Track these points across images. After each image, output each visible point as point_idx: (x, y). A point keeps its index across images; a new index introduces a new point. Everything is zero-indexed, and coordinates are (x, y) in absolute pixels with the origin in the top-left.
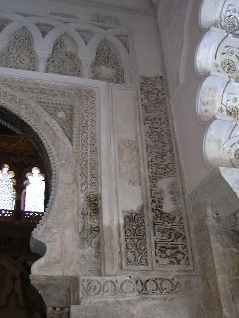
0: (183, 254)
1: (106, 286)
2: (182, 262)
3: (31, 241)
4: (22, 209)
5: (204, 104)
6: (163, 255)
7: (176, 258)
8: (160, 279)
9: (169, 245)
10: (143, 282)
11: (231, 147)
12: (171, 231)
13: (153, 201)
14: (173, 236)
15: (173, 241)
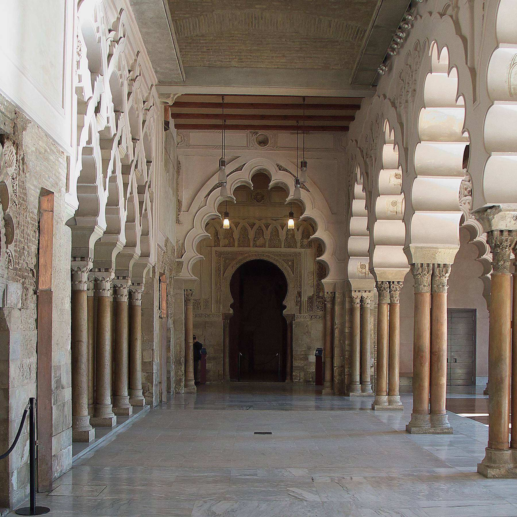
6: (318, 309)
13: (317, 293)
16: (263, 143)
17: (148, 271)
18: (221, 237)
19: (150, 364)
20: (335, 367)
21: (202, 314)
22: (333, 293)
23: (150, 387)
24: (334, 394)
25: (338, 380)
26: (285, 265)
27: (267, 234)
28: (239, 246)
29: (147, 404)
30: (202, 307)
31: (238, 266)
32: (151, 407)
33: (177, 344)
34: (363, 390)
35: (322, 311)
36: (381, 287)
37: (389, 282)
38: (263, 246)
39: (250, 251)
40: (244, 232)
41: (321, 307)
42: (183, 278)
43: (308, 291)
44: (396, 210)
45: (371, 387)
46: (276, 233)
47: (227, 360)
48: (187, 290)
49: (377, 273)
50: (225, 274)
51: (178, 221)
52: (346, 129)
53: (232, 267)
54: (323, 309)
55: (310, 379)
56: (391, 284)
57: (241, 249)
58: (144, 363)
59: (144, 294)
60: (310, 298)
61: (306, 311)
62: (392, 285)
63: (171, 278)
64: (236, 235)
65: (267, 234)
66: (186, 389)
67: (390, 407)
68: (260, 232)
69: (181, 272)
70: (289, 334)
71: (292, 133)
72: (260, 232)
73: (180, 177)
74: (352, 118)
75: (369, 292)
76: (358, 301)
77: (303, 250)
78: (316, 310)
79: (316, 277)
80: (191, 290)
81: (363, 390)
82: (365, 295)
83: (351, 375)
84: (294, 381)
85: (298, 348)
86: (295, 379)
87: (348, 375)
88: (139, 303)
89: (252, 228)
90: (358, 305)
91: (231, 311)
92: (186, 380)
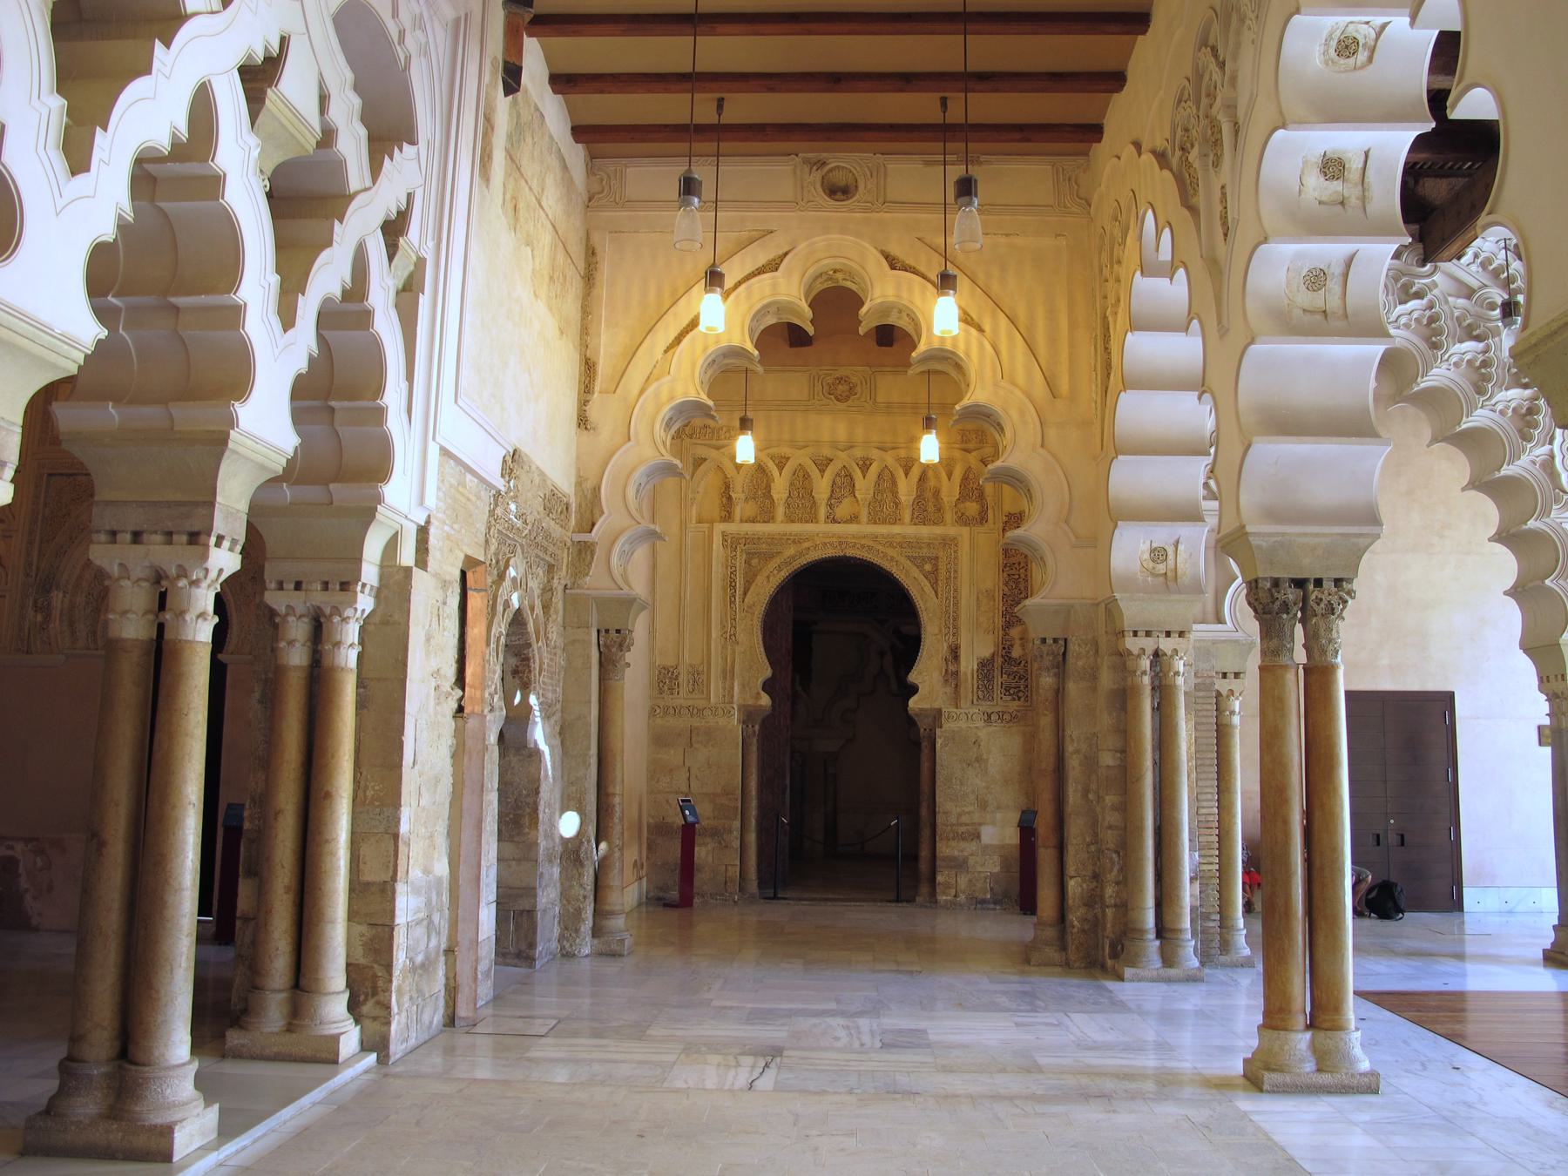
2: (1022, 699)
6: (1007, 693)
9: (1013, 685)
13: (1004, 648)
16: (839, 191)
17: (392, 546)
18: (737, 494)
19: (383, 891)
20: (1071, 877)
21: (681, 707)
22: (1062, 642)
23: (380, 983)
24: (1067, 966)
25: (1083, 920)
26: (915, 572)
27: (864, 486)
28: (790, 519)
29: (365, 1047)
30: (684, 690)
31: (784, 574)
32: (383, 1059)
33: (569, 800)
34: (1168, 959)
35: (1019, 700)
36: (1273, 603)
37: (1300, 583)
38: (854, 519)
39: (818, 535)
40: (802, 485)
41: (1015, 688)
42: (593, 593)
43: (977, 648)
44: (1322, 304)
45: (1192, 950)
46: (886, 482)
47: (752, 837)
48: (607, 631)
49: (1260, 547)
50: (748, 596)
51: (583, 422)
52: (1092, 132)
53: (768, 577)
54: (1021, 694)
55: (985, 893)
56: (1311, 587)
57: (796, 528)
58: (357, 887)
59: (375, 624)
60: (985, 666)
61: (975, 700)
62: (1316, 593)
63: (549, 590)
64: (780, 486)
65: (864, 486)
66: (596, 941)
67: (1326, 1078)
68: (844, 485)
69: (587, 575)
70: (925, 765)
71: (927, 163)
72: (844, 485)
73: (595, 292)
74: (1115, 80)
75: (1181, 634)
76: (1145, 663)
77: (965, 531)
78: (1001, 698)
79: (1001, 605)
80: (618, 631)
81: (1168, 959)
82: (1166, 645)
83: (1126, 907)
84: (939, 898)
85: (954, 804)
86: (944, 893)
87: (1116, 906)
88: (349, 657)
89: (822, 471)
90: (1146, 680)
91: (765, 700)
92: (598, 913)
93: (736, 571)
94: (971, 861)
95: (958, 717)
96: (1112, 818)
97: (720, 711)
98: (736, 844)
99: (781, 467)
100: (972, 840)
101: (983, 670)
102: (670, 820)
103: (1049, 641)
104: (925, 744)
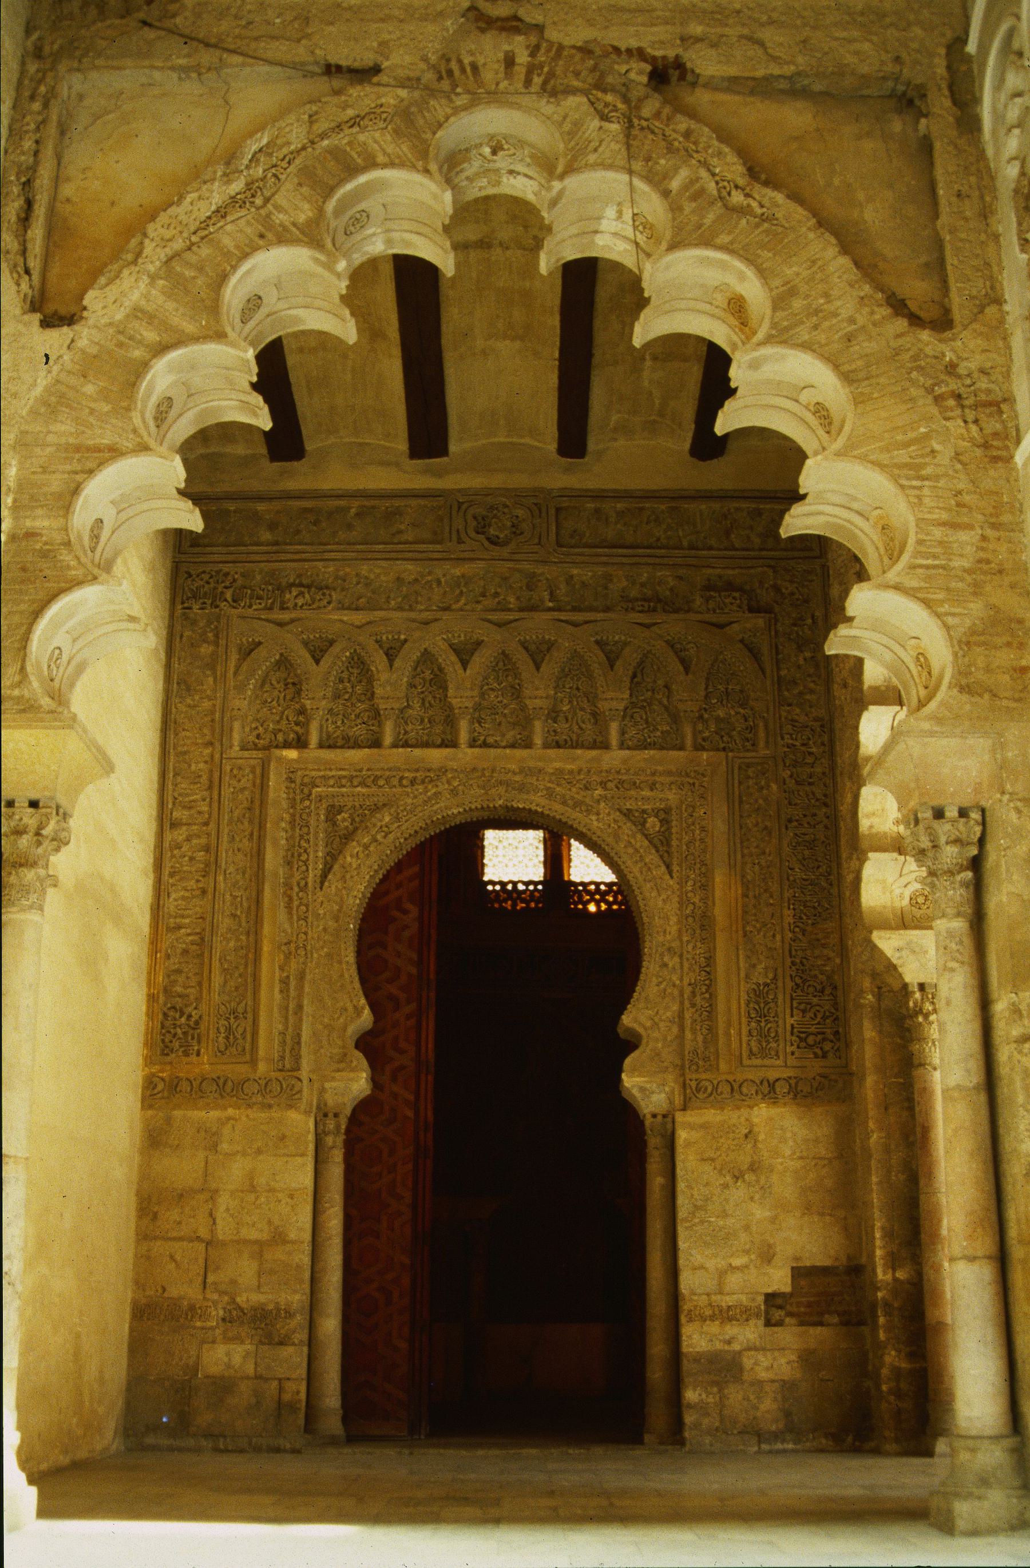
0: (832, 1041)
1: (720, 1086)
2: (831, 1055)
3: (619, 1026)
4: (566, 878)
5: (868, 816)
6: (803, 1044)
7: (821, 1049)
8: (795, 1078)
9: (813, 1029)
10: (771, 1082)
11: (905, 886)
12: (818, 1008)
13: (793, 963)
14: (819, 1016)
15: (818, 1023)
22: (975, 815)
54: (827, 1046)
70: (656, 1182)
80: (34, 804)
93: (308, 834)
94: (747, 1362)
95: (715, 1088)
96: (892, 1358)
97: (275, 1087)
98: (302, 1336)
99: (391, 656)
100: (747, 1320)
101: (758, 1003)
102: (173, 1292)
103: (952, 813)
104: (654, 1142)
